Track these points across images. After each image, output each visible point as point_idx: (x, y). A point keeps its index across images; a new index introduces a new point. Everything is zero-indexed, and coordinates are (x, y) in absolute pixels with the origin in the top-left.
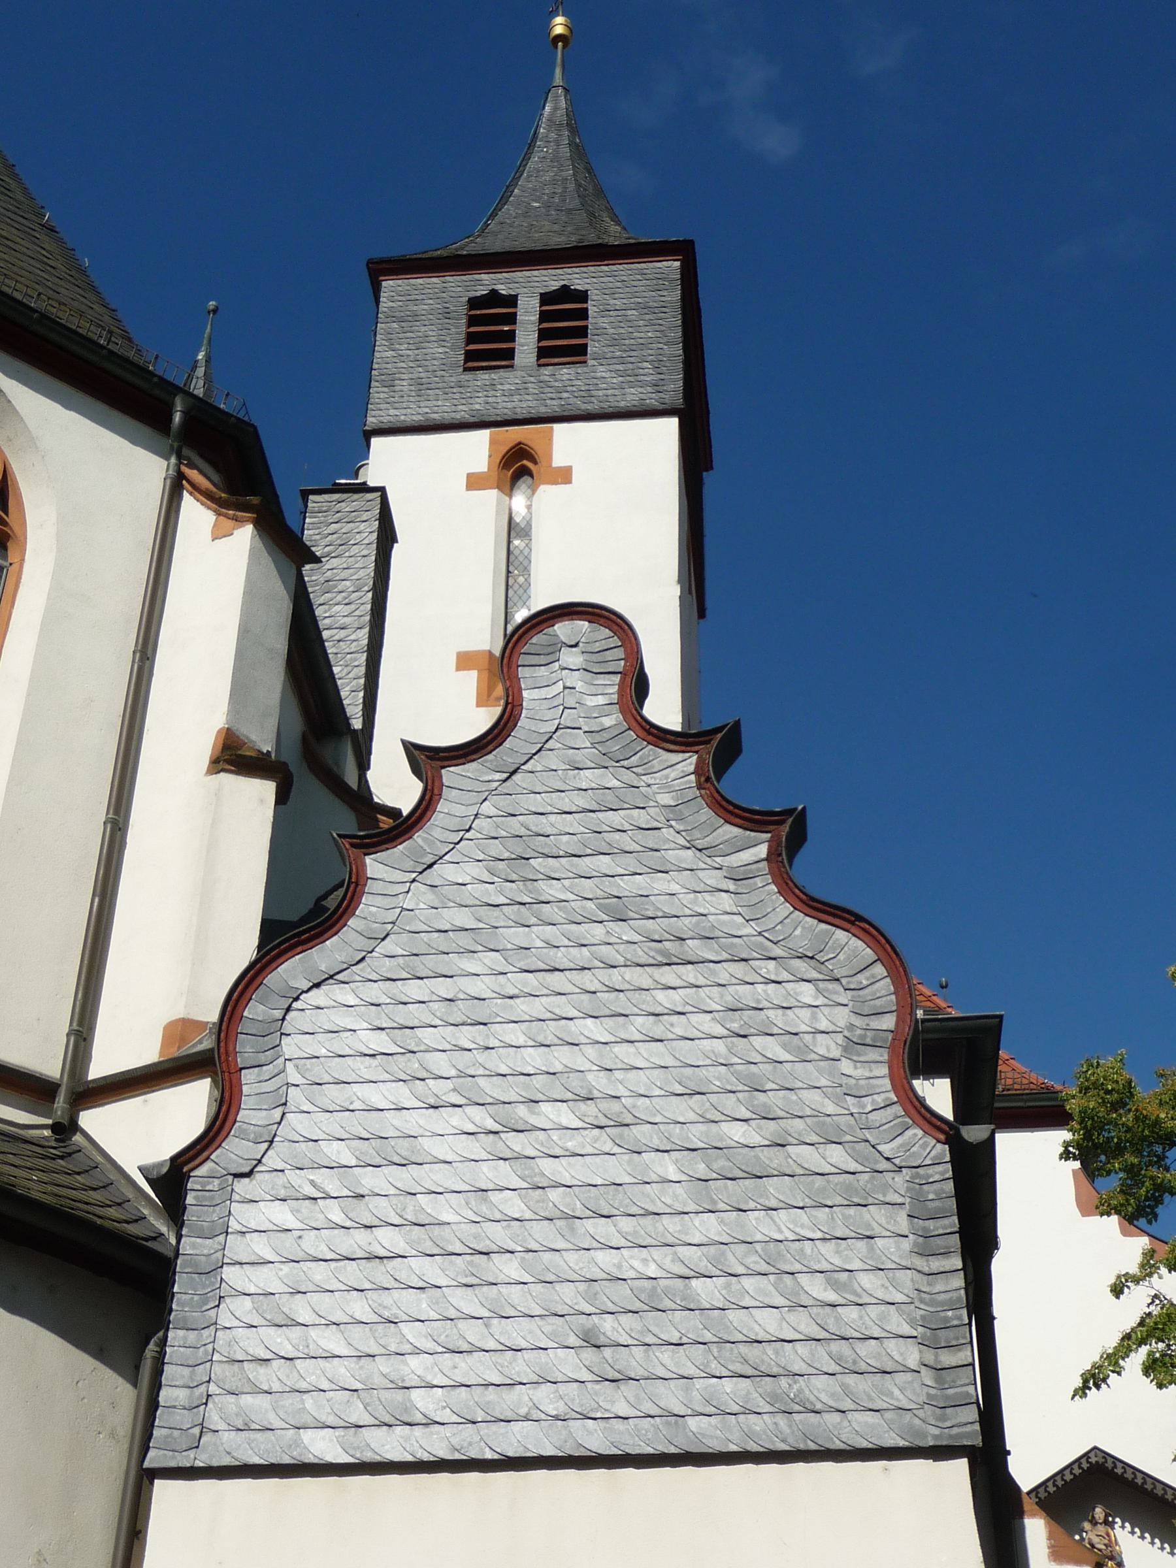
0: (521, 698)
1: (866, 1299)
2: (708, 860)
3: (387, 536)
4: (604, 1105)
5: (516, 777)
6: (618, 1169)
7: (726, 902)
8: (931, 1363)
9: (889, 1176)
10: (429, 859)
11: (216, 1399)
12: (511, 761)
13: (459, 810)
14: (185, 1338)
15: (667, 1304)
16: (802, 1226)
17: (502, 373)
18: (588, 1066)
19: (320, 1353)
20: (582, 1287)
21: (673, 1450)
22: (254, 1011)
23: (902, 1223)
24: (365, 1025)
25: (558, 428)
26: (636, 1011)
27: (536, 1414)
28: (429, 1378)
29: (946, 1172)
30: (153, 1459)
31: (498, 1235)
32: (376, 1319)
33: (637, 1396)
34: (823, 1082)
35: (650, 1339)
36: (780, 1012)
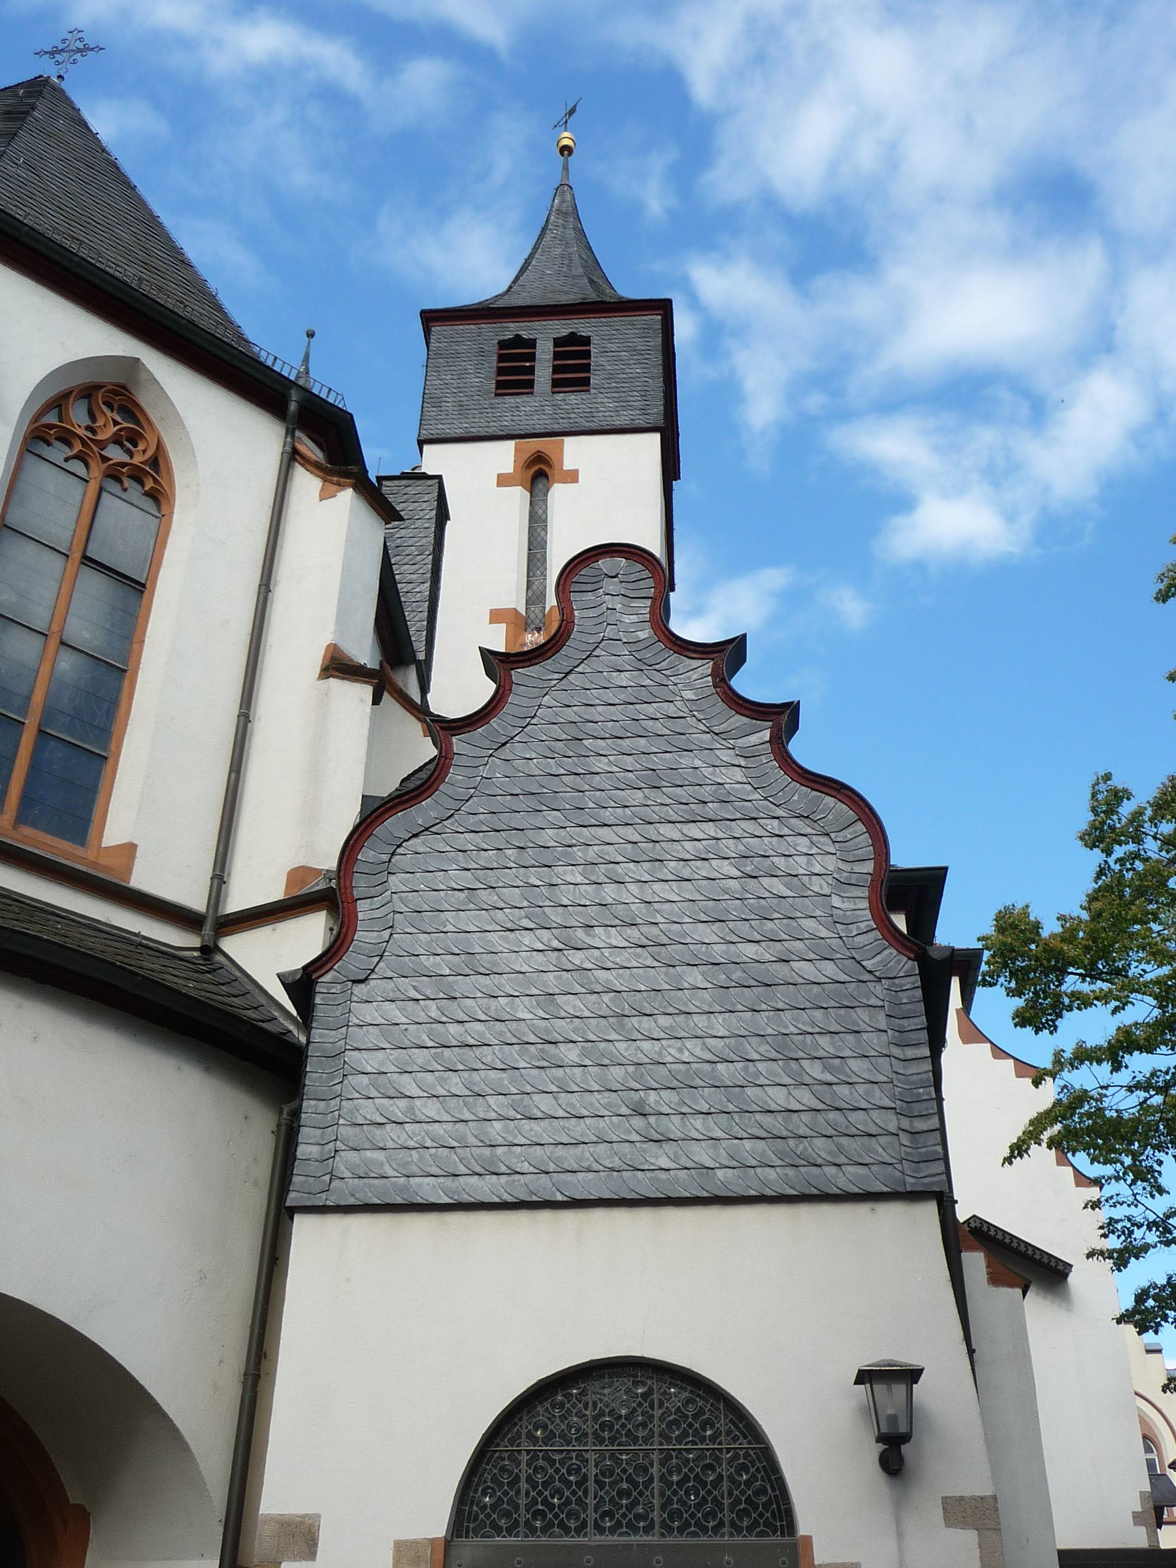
1: (855, 1079)
2: (724, 742)
3: (442, 515)
4: (645, 929)
7: (738, 774)
8: (908, 1128)
9: (871, 985)
10: (503, 739)
11: (342, 1154)
13: (525, 702)
14: (316, 1106)
15: (699, 1082)
16: (804, 1023)
17: (524, 398)
18: (632, 899)
19: (423, 1118)
20: (631, 1069)
21: (705, 1194)
22: (367, 855)
23: (882, 1023)
24: (455, 867)
25: (569, 441)
26: (669, 857)
27: (596, 1167)
28: (511, 1139)
29: (916, 981)
30: (292, 1199)
31: (563, 1028)
32: (468, 1093)
33: (676, 1153)
34: (818, 913)
35: (685, 1109)
36: (783, 859)
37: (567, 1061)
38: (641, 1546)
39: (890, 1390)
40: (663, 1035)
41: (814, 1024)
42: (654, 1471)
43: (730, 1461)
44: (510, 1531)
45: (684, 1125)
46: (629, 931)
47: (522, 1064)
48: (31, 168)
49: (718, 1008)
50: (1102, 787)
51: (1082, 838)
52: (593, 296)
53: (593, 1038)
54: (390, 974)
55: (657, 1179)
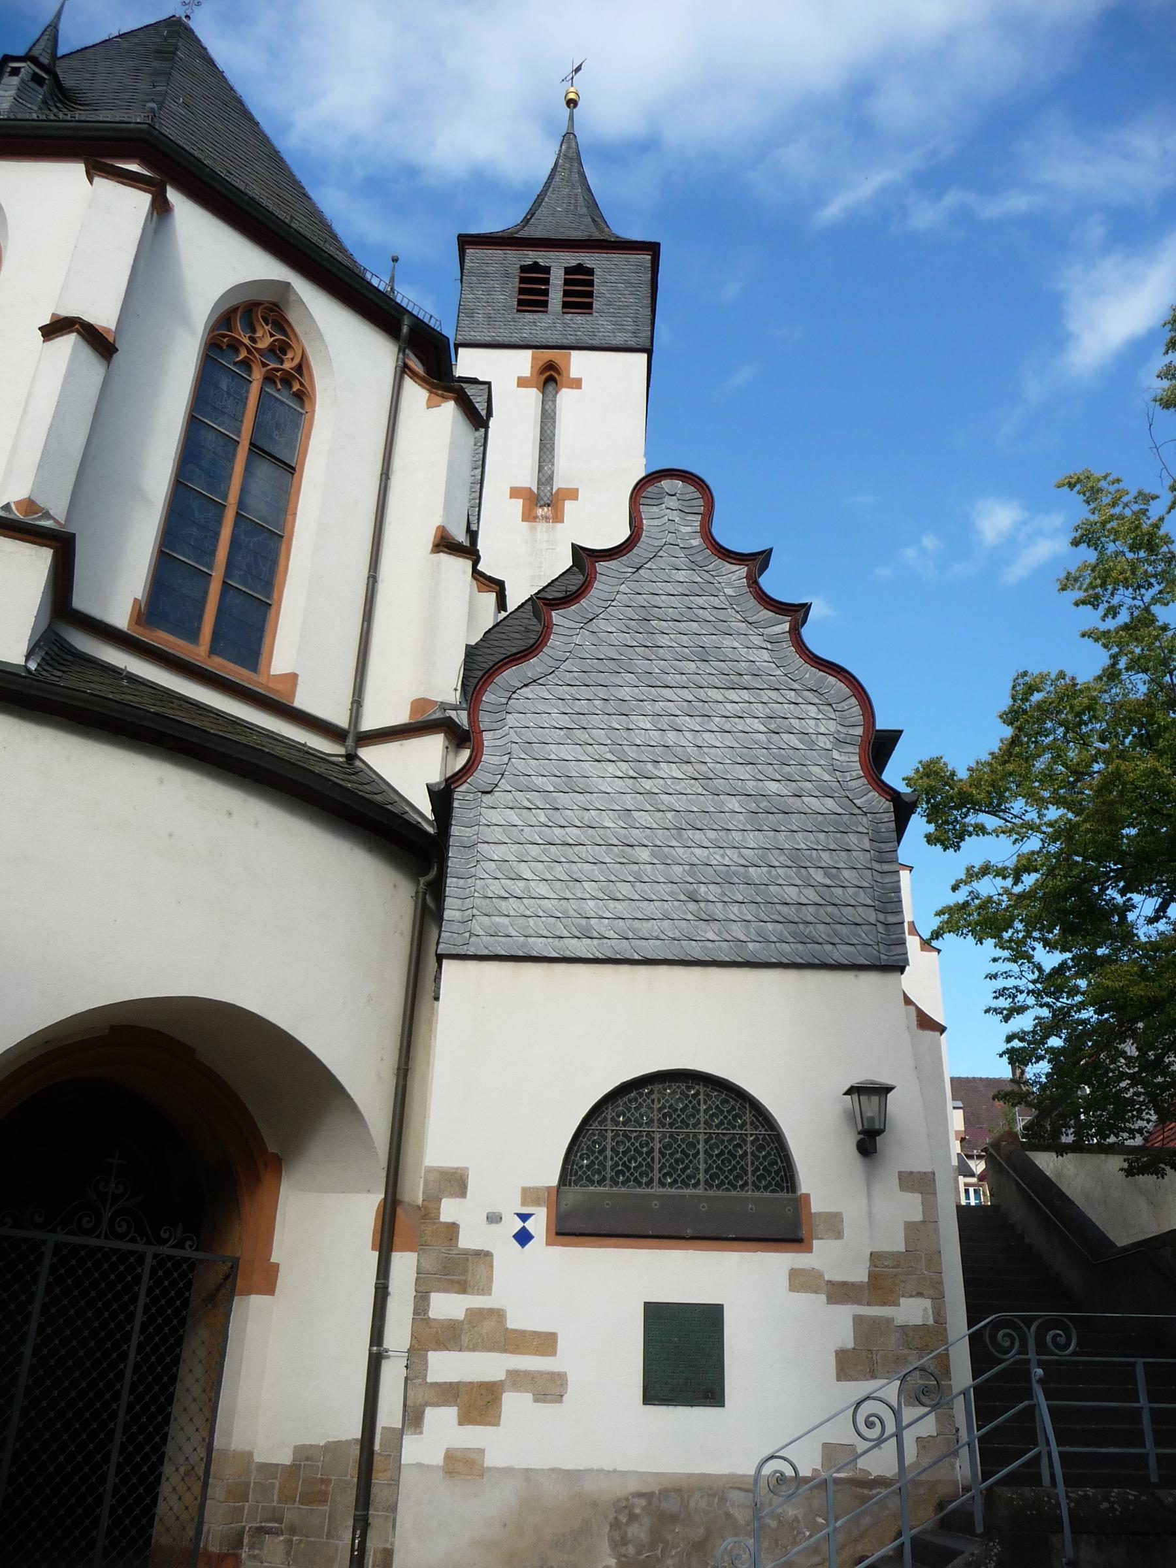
0: (642, 523)
4: (697, 766)
5: (641, 571)
6: (709, 803)
7: (766, 655)
9: (860, 817)
12: (638, 561)
15: (736, 880)
18: (687, 744)
19: (537, 895)
20: (687, 868)
21: (740, 960)
23: (867, 844)
25: (575, 355)
34: (822, 762)
35: (726, 899)
37: (641, 860)
38: (692, 1196)
39: (870, 1101)
40: (710, 845)
41: (818, 843)
42: (700, 1147)
43: (753, 1142)
44: (600, 1183)
45: (725, 910)
46: (685, 767)
47: (608, 860)
48: (186, 105)
49: (750, 827)
50: (1021, 681)
51: (1001, 717)
52: (597, 235)
53: (660, 844)
54: (509, 788)
55: (706, 947)
